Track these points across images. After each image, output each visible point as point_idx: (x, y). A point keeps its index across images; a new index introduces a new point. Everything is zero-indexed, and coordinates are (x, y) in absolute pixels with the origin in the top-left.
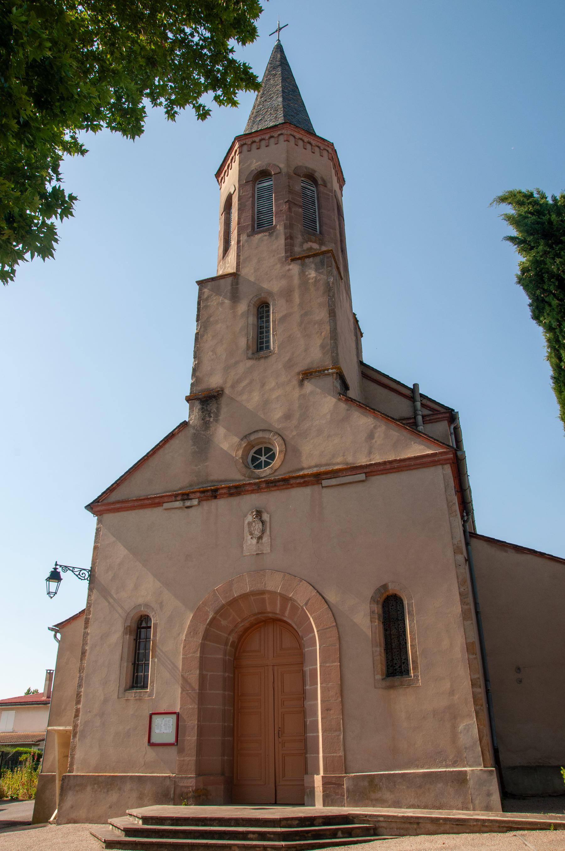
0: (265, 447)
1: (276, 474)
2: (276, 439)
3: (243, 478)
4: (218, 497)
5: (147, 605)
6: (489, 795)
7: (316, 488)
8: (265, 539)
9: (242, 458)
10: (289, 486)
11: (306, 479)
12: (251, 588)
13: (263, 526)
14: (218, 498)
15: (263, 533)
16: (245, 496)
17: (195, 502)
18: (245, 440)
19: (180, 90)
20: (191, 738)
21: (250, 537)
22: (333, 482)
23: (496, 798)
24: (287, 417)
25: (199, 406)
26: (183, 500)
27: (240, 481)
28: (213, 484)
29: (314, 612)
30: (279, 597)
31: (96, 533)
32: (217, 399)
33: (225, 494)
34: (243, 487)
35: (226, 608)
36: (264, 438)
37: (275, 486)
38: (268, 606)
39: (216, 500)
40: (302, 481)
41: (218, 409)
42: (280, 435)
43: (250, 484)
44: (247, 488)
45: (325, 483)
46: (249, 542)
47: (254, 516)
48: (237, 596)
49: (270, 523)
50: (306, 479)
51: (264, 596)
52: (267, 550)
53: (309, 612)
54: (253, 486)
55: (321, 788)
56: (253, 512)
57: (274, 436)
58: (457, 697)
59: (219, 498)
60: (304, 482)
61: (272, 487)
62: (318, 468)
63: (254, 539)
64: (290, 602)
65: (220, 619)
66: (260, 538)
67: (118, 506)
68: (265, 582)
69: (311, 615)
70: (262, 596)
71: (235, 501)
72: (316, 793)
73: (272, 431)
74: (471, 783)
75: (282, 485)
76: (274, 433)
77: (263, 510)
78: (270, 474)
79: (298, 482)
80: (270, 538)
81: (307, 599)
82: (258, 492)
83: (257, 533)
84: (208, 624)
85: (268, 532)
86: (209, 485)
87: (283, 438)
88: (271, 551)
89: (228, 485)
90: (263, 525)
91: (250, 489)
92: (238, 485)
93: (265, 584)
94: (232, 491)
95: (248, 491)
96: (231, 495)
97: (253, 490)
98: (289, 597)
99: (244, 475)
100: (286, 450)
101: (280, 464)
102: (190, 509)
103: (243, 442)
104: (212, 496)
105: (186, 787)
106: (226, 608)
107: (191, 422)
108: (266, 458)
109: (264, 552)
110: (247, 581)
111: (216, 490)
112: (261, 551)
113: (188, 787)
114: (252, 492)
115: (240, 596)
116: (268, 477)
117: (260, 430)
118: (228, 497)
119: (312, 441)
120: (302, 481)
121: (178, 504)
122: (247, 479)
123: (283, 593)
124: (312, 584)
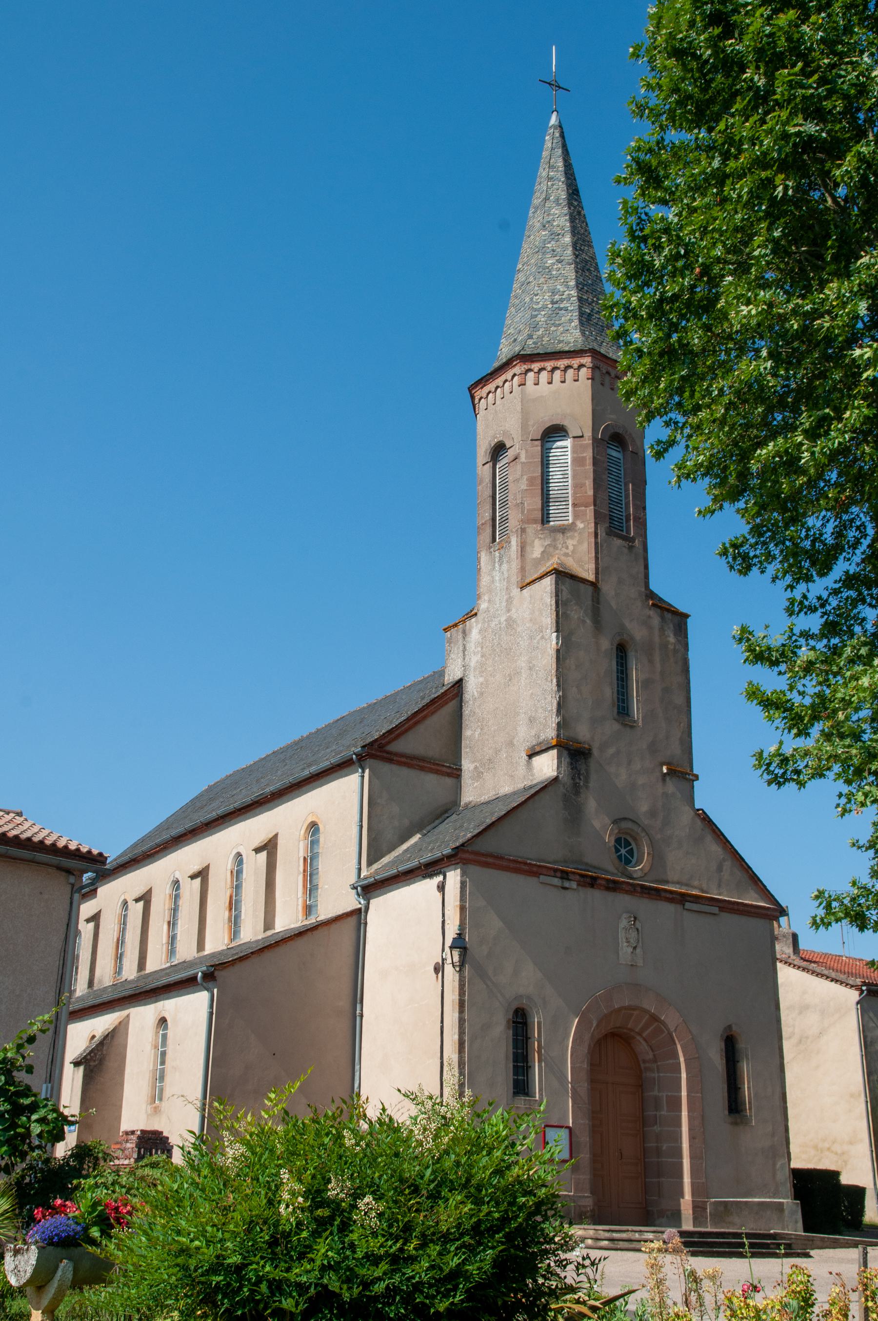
3: (616, 871)
5: (529, 998)
6: (796, 1222)
7: (679, 907)
8: (638, 950)
17: (574, 885)
19: (712, 171)
20: (585, 1156)
22: (695, 907)
23: (800, 1224)
24: (653, 813)
25: (568, 760)
26: (562, 878)
31: (461, 888)
32: (585, 759)
37: (649, 893)
40: (671, 896)
41: (588, 771)
44: (688, 898)
45: (688, 905)
52: (640, 963)
55: (691, 1212)
58: (776, 1139)
66: (635, 948)
67: (490, 860)
71: (610, 896)
72: (683, 1216)
74: (786, 1212)
85: (640, 944)
86: (583, 867)
96: (608, 889)
99: (617, 869)
102: (567, 892)
105: (584, 1206)
107: (561, 776)
111: (594, 879)
113: (585, 1207)
114: (627, 892)
117: (631, 820)
120: (671, 896)
121: (556, 881)
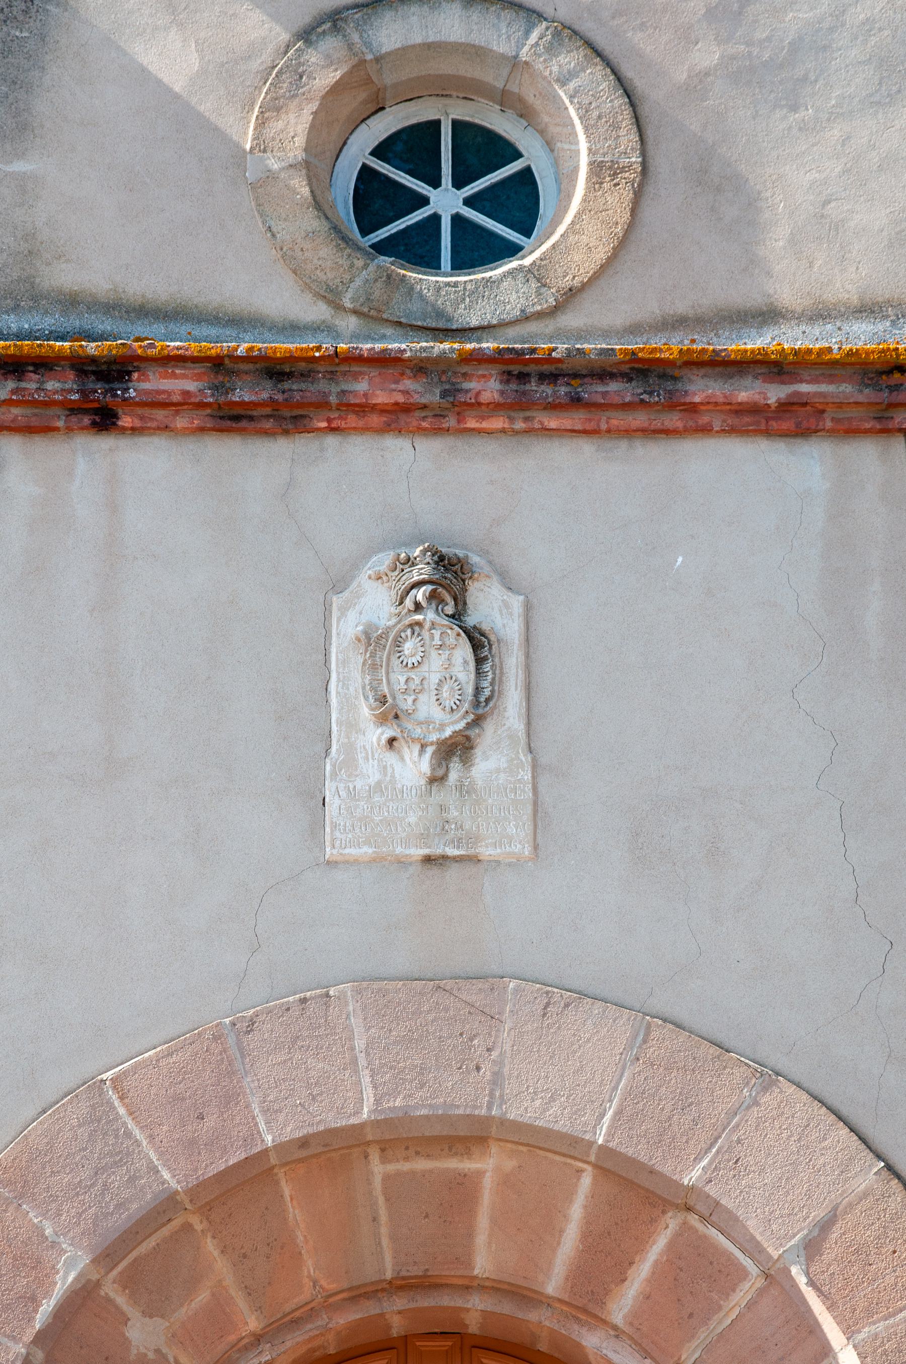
0: (456, 124)
1: (571, 320)
2: (572, 75)
4: (125, 421)
9: (308, 166)
10: (673, 420)
11: (804, 388)
12: (394, 1093)
13: (479, 673)
14: (123, 430)
15: (478, 721)
16: (331, 441)
18: (330, 44)
21: (377, 735)
27: (293, 328)
28: (74, 322)
29: (869, 1312)
30: (586, 1181)
33: (186, 403)
34: (332, 376)
35: (176, 1224)
36: (476, 53)
37: (576, 402)
38: (481, 1239)
39: (104, 443)
40: (775, 393)
42: (599, 54)
43: (383, 361)
46: (370, 772)
47: (420, 594)
48: (279, 1147)
49: (527, 656)
50: (804, 388)
51: (468, 1165)
53: (831, 1307)
54: (408, 384)
56: (409, 562)
57: (550, 50)
59: (134, 431)
60: (786, 407)
61: (553, 407)
62: (882, 326)
63: (410, 753)
64: (672, 1223)
65: (121, 1300)
68: (500, 1063)
69: (849, 1332)
70: (453, 1164)
73: (541, 16)
75: (626, 406)
76: (557, 34)
77: (475, 559)
78: (525, 318)
79: (743, 396)
80: (525, 759)
81: (819, 1213)
82: (438, 431)
83: (438, 714)
84: (40, 1338)
86: (47, 323)
87: (619, 79)
88: (536, 847)
89: (214, 349)
90: (480, 661)
91: (381, 398)
92: (291, 358)
93: (497, 1079)
94: (242, 394)
95: (363, 409)
97: (406, 409)
98: (678, 1185)
100: (644, 164)
101: (601, 254)
103: (313, 57)
104: (73, 410)
106: (176, 1224)
108: (468, 202)
109: (486, 851)
110: (360, 1043)
112: (458, 842)
115: (304, 1142)
116: (511, 332)
118: (202, 430)
119: (836, 133)
120: (775, 393)
122: (350, 323)
123: (639, 1151)
124: (845, 1111)
